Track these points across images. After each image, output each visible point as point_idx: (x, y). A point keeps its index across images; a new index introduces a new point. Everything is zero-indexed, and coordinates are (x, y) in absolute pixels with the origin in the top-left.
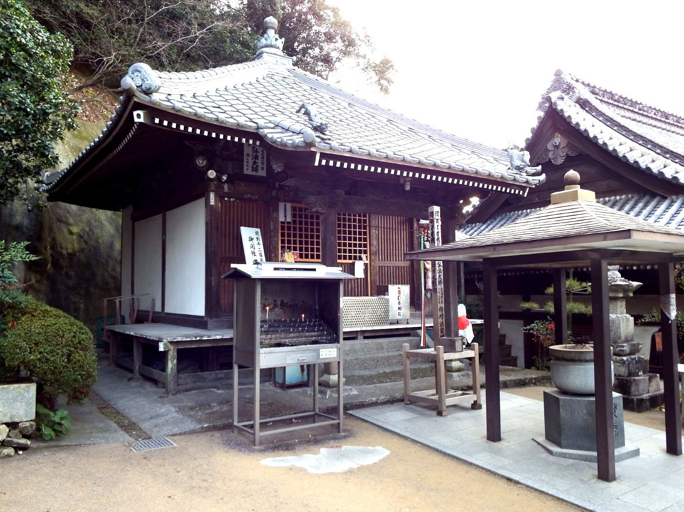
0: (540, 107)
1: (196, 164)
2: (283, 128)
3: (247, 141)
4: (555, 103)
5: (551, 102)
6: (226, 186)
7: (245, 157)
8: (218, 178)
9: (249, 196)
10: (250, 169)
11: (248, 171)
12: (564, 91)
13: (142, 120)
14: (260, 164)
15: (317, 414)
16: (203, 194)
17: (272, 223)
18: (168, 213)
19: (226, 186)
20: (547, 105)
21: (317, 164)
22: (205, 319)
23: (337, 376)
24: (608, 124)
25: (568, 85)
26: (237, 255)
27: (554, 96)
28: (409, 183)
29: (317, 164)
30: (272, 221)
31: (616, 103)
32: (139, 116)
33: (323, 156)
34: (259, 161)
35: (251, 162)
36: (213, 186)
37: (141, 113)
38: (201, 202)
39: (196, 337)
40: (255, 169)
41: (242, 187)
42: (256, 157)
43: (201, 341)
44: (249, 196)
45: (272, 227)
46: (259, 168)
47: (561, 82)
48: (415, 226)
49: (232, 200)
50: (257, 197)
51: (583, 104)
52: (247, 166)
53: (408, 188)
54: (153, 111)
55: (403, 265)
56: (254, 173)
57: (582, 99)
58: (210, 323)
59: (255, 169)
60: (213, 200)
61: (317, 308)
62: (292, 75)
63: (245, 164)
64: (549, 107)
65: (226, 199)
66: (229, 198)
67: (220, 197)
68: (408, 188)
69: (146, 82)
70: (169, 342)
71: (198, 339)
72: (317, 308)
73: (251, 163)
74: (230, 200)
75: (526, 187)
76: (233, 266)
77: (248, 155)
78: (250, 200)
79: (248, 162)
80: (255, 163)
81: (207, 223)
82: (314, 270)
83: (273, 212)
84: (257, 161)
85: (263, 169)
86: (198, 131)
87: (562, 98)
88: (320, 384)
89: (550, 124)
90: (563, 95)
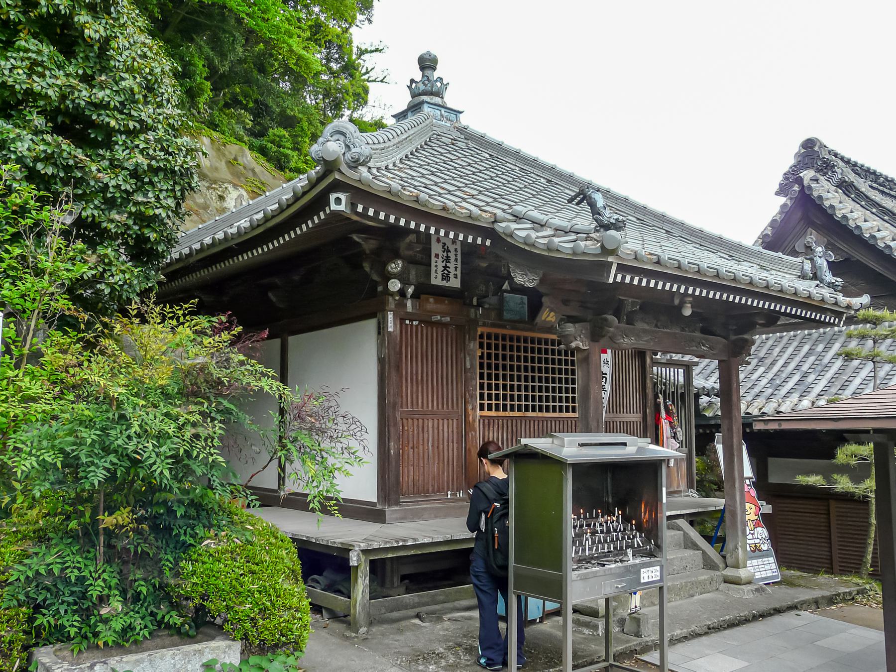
0: (783, 190)
1: (400, 271)
2: (533, 222)
3: (437, 232)
4: (810, 188)
5: (803, 186)
6: (409, 303)
7: (433, 259)
8: (402, 293)
9: (439, 318)
10: (440, 276)
11: (436, 280)
12: (818, 171)
13: (342, 207)
14: (452, 270)
15: (611, 665)
16: (376, 312)
17: (468, 359)
18: (293, 340)
19: (409, 303)
20: (796, 188)
21: (611, 281)
22: (378, 507)
23: (657, 608)
24: (886, 218)
25: (825, 162)
26: (422, 407)
27: (807, 175)
28: (689, 305)
29: (611, 281)
30: (469, 355)
31: (881, 188)
32: (339, 203)
33: (622, 268)
34: (451, 265)
35: (441, 265)
36: (391, 303)
37: (343, 197)
38: (372, 324)
39: (397, 542)
40: (446, 277)
41: (431, 303)
42: (447, 260)
43: (404, 547)
44: (439, 318)
45: (468, 365)
46: (452, 276)
47: (815, 156)
48: (648, 360)
49: (414, 323)
50: (449, 319)
51: (846, 187)
52: (436, 272)
53: (687, 312)
54: (359, 193)
55: (632, 420)
56: (444, 283)
57: (845, 182)
58: (390, 511)
59: (446, 277)
60: (392, 325)
61: (610, 500)
62: (463, 137)
63: (433, 269)
64: (800, 191)
65: (407, 322)
66: (411, 321)
67: (401, 319)
68: (687, 312)
69: (353, 150)
70: (362, 551)
71: (401, 544)
72: (610, 500)
73: (440, 269)
74: (412, 325)
75: (844, 313)
76: (524, 441)
77: (437, 256)
78: (438, 324)
79: (436, 266)
80: (445, 267)
81: (381, 361)
82: (625, 444)
83: (470, 342)
84: (448, 265)
85: (456, 277)
86: (413, 225)
87: (817, 180)
88: (575, 611)
89: (799, 215)
90: (818, 175)
